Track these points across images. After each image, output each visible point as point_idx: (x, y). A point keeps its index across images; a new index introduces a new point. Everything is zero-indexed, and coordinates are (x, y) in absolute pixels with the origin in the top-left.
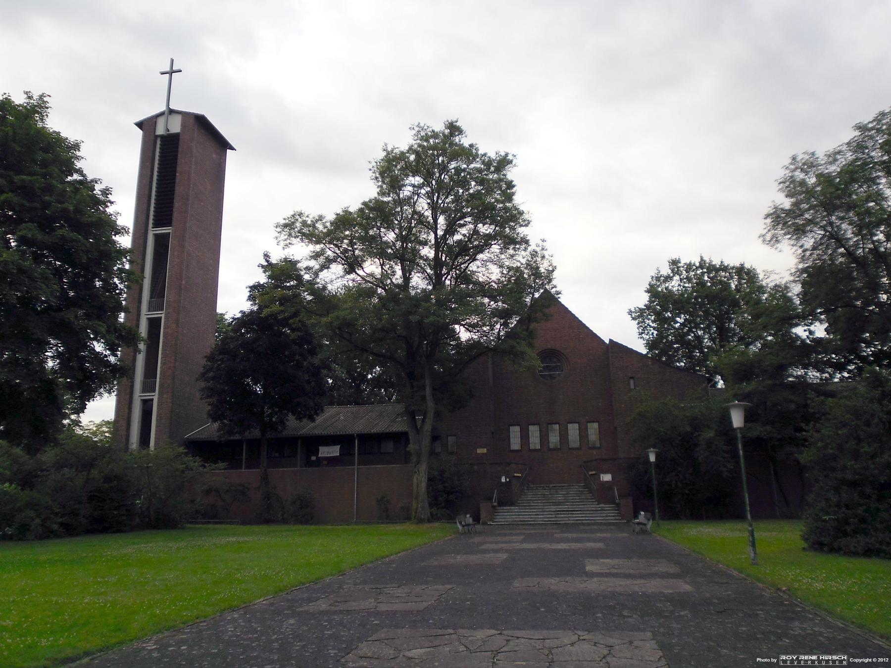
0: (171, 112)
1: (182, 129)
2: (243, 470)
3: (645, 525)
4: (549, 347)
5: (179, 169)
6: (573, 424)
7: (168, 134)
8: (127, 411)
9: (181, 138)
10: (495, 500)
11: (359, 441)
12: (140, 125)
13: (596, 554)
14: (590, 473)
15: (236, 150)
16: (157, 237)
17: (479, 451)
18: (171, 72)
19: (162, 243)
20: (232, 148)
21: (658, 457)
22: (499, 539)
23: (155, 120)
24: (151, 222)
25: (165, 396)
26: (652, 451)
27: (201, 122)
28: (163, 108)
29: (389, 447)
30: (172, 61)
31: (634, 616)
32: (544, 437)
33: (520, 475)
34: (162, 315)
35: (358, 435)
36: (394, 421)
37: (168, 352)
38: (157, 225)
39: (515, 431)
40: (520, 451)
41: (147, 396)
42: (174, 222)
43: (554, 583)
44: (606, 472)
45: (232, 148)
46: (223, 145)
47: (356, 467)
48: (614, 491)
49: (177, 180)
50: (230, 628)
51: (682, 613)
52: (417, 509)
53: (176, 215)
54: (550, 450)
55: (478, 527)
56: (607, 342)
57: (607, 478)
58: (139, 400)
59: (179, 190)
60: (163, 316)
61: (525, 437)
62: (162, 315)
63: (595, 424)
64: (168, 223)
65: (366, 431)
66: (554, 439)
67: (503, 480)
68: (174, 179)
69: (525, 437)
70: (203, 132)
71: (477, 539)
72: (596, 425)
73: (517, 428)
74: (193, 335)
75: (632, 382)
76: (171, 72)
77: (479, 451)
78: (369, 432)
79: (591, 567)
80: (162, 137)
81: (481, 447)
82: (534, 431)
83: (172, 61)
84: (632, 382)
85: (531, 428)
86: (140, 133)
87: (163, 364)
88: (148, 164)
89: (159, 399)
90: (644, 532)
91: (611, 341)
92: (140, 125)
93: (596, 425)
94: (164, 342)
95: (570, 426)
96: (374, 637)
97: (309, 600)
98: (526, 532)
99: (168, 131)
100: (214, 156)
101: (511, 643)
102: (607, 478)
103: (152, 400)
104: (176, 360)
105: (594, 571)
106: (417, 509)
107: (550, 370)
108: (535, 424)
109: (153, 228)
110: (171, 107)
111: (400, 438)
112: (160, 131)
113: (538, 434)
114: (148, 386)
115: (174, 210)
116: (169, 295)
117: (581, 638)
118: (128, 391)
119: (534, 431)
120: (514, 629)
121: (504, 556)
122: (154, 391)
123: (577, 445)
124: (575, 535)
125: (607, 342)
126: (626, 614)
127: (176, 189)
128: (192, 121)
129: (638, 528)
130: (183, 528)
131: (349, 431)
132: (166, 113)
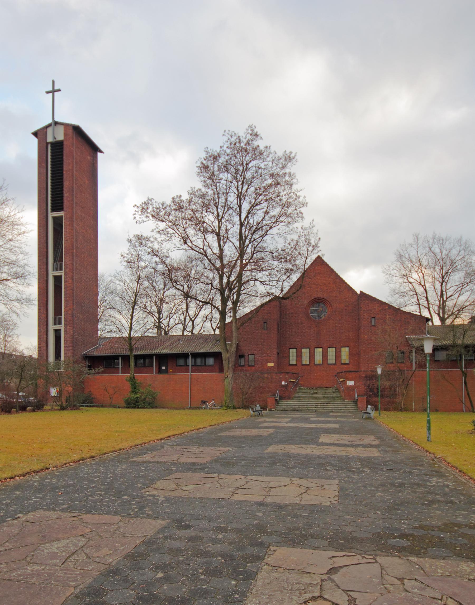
0: (56, 123)
1: (64, 138)
2: (120, 375)
3: (370, 413)
4: (319, 296)
5: (65, 168)
6: (332, 348)
7: (55, 141)
8: (45, 337)
9: (65, 143)
10: (277, 395)
11: (192, 357)
12: (35, 134)
13: (328, 431)
14: (340, 380)
15: (104, 153)
16: (55, 219)
17: (269, 365)
18: (53, 92)
19: (58, 223)
20: (101, 152)
21: (383, 371)
22: (275, 420)
23: (45, 130)
24: (50, 208)
25: (68, 327)
26: (380, 367)
27: (77, 130)
28: (50, 121)
29: (181, 362)
30: (53, 82)
31: (333, 470)
32: (312, 356)
33: (294, 380)
34: (61, 273)
35: (191, 353)
36: (214, 345)
37: (68, 299)
38: (53, 210)
39: (293, 352)
40: (296, 365)
41: (57, 327)
42: (65, 208)
43: (293, 449)
44: (351, 380)
45: (101, 152)
46: (95, 149)
47: (190, 374)
48: (355, 392)
49: (64, 177)
50: (86, 469)
51: (364, 469)
52: (226, 401)
53: (66, 203)
54: (316, 365)
55: (264, 412)
56: (359, 293)
57: (351, 383)
58: (52, 330)
59: (66, 184)
60: (63, 274)
61: (299, 356)
62: (61, 273)
63: (333, 348)
64: (61, 209)
65: (196, 351)
66: (319, 358)
67: (283, 383)
68: (63, 175)
69: (299, 356)
70: (80, 139)
71: (261, 420)
72: (347, 349)
73: (295, 351)
74: (83, 287)
75: (373, 320)
76: (53, 92)
77: (269, 365)
78: (198, 352)
79: (324, 439)
80: (51, 143)
81: (270, 362)
82: (306, 352)
83: (53, 82)
84: (373, 320)
85: (304, 350)
86: (35, 141)
87: (66, 306)
88: (44, 164)
89: (65, 329)
90: (369, 418)
91: (361, 292)
92: (35, 134)
93: (347, 349)
94: (65, 293)
95: (330, 350)
96: (168, 478)
97: (140, 454)
98: (293, 416)
99: (55, 138)
100: (89, 158)
101: (249, 484)
102: (351, 383)
103: (60, 330)
104: (73, 304)
105: (323, 442)
106: (226, 401)
107: (318, 312)
108: (306, 348)
109: (51, 212)
110: (57, 119)
111: (217, 356)
112: (50, 139)
113: (308, 354)
114: (57, 321)
115: (64, 199)
116: (66, 260)
117: (293, 482)
118: (45, 323)
119: (306, 352)
120: (254, 475)
121: (271, 431)
122: (61, 324)
123: (334, 362)
124: (323, 419)
125: (359, 293)
126: (329, 469)
127: (64, 183)
128: (71, 131)
129: (365, 416)
130: (79, 409)
131: (186, 352)
132: (53, 125)
